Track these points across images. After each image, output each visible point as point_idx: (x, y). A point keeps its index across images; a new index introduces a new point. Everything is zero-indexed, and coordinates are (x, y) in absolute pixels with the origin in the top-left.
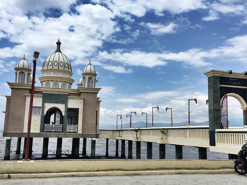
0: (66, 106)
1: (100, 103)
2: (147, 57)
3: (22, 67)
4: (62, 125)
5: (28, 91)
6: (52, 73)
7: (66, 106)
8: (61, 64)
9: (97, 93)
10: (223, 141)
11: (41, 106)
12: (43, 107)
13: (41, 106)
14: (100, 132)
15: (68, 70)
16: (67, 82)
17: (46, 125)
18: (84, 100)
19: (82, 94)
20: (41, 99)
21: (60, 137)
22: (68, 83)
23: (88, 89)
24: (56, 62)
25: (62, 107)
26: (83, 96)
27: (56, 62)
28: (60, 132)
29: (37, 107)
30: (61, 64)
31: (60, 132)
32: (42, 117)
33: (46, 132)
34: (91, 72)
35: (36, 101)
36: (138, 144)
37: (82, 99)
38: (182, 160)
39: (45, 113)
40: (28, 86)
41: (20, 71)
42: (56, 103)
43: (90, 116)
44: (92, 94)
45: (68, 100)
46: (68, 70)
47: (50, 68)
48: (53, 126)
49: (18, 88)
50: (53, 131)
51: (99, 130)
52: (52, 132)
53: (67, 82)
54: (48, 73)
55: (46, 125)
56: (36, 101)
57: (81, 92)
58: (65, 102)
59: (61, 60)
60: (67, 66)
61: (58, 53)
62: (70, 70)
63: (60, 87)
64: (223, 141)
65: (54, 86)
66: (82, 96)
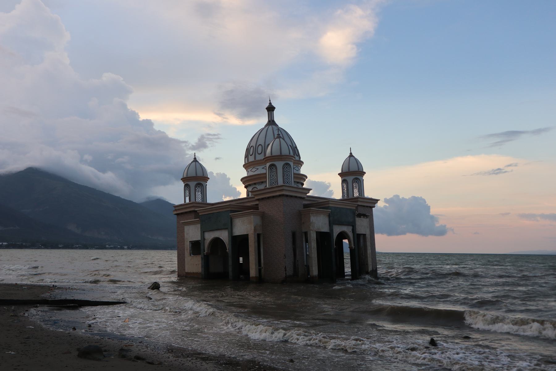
7: (231, 232)
25: (224, 235)
58: (230, 227)
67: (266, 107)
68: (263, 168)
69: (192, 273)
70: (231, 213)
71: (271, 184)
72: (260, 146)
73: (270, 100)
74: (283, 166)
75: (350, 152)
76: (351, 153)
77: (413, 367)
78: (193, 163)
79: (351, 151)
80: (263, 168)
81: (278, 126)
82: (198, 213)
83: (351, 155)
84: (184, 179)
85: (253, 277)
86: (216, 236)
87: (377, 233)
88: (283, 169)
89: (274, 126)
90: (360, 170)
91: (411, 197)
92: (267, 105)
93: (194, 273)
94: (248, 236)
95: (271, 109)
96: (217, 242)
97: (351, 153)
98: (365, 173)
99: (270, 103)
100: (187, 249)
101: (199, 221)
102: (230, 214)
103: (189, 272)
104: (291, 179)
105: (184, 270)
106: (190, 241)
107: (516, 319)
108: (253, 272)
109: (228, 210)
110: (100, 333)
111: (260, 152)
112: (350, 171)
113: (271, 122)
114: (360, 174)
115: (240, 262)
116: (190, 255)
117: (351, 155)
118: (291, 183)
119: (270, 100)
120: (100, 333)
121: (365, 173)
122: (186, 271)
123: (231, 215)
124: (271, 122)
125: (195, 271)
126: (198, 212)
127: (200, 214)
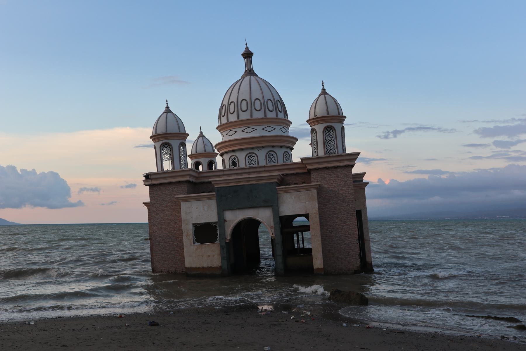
0: (276, 212)
1: (365, 189)
2: (318, 224)
3: (326, 115)
5: (185, 187)
8: (258, 103)
9: (356, 159)
15: (277, 116)
16: (277, 146)
18: (320, 190)
19: (313, 175)
20: (213, 203)
22: (281, 147)
23: (329, 159)
24: (244, 102)
26: (316, 180)
27: (269, 102)
30: (258, 103)
32: (222, 247)
34: (328, 113)
35: (204, 209)
37: (312, 188)
39: (228, 237)
40: (165, 178)
44: (339, 170)
47: (245, 116)
49: (161, 184)
53: (277, 146)
56: (204, 209)
57: (309, 171)
59: (257, 94)
60: (271, 108)
61: (247, 78)
65: (247, 161)
67: (242, 53)
68: (262, 129)
69: (199, 268)
72: (244, 102)
73: (246, 44)
75: (166, 106)
76: (168, 108)
78: (164, 114)
79: (167, 104)
80: (262, 129)
81: (257, 76)
82: (213, 185)
83: (168, 110)
84: (155, 137)
85: (318, 269)
86: (249, 216)
87: (141, 225)
89: (252, 77)
91: (48, 172)
92: (243, 50)
93: (203, 268)
94: (308, 216)
95: (248, 55)
97: (168, 108)
98: (188, 135)
99: (247, 48)
100: (188, 235)
101: (215, 196)
102: (277, 187)
103: (194, 266)
105: (183, 262)
106: (193, 224)
108: (318, 262)
109: (272, 183)
112: (168, 132)
113: (250, 72)
115: (296, 248)
116: (194, 243)
117: (168, 110)
119: (246, 44)
121: (188, 135)
122: (187, 265)
123: (278, 189)
124: (250, 72)
125: (205, 265)
126: (213, 183)
127: (215, 186)
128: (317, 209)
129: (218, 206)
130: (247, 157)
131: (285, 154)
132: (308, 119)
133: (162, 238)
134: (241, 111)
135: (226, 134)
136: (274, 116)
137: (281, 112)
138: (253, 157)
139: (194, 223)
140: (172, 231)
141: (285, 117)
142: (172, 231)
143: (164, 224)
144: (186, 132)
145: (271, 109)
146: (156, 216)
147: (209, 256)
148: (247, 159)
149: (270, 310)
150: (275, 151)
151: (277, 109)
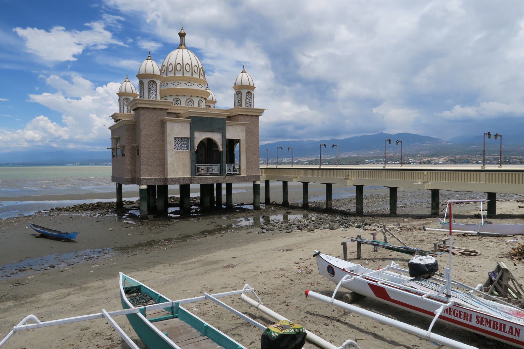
4: (219, 164)
6: (196, 84)
7: (224, 136)
8: (179, 66)
10: (339, 175)
11: (189, 136)
12: (192, 139)
13: (189, 136)
14: (261, 170)
15: (200, 77)
17: (198, 165)
20: (188, 126)
21: (220, 182)
25: (217, 137)
27: (188, 65)
28: (217, 175)
29: (184, 138)
30: (179, 66)
31: (217, 175)
33: (199, 175)
36: (219, 186)
38: (43, 228)
39: (196, 148)
40: (164, 105)
41: (150, 80)
42: (210, 131)
43: (252, 150)
45: (226, 126)
46: (200, 77)
48: (208, 166)
50: (208, 173)
51: (260, 168)
52: (206, 175)
54: (176, 84)
55: (198, 165)
58: (222, 131)
60: (196, 71)
62: (202, 78)
63: (196, 105)
64: (339, 175)
65: (187, 104)
66: (240, 121)
68: (185, 84)
70: (167, 117)
71: (499, 156)
74: (246, 94)
77: (425, 233)
80: (185, 84)
88: (246, 95)
90: (250, 85)
96: (210, 141)
98: (255, 88)
104: (251, 103)
107: (450, 326)
110: (494, 161)
111: (170, 70)
114: (252, 88)
118: (251, 106)
120: (494, 161)
121: (255, 88)
128: (245, 137)
129: (191, 128)
130: (187, 101)
131: (200, 102)
132: (138, 74)
133: (148, 145)
134: (185, 71)
135: (168, 84)
136: (173, 75)
137: (202, 75)
138: (191, 101)
139: (175, 137)
140: (155, 140)
141: (204, 79)
142: (155, 140)
143: (150, 135)
144: (254, 86)
145: (196, 72)
146: (144, 130)
147: (183, 159)
148: (187, 102)
149: (146, 242)
150: (193, 99)
151: (200, 73)
